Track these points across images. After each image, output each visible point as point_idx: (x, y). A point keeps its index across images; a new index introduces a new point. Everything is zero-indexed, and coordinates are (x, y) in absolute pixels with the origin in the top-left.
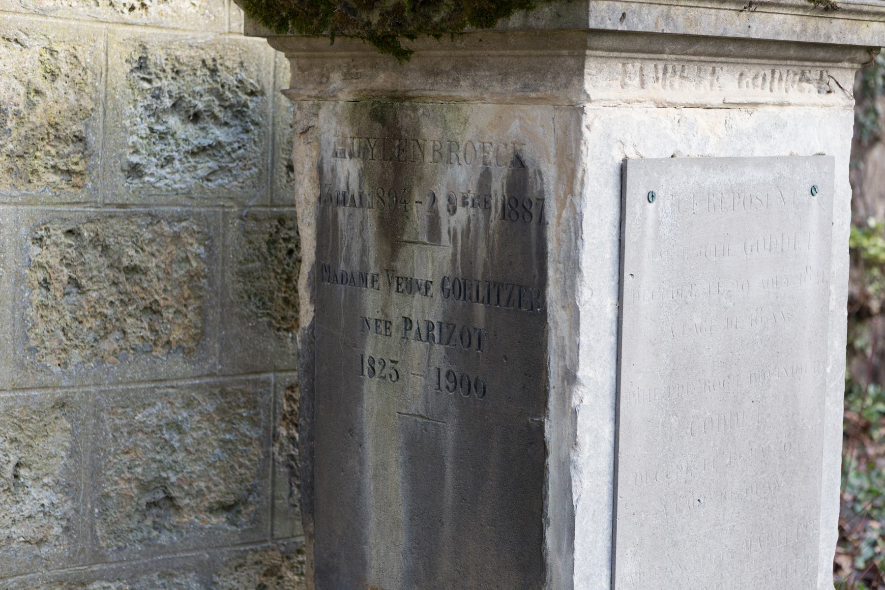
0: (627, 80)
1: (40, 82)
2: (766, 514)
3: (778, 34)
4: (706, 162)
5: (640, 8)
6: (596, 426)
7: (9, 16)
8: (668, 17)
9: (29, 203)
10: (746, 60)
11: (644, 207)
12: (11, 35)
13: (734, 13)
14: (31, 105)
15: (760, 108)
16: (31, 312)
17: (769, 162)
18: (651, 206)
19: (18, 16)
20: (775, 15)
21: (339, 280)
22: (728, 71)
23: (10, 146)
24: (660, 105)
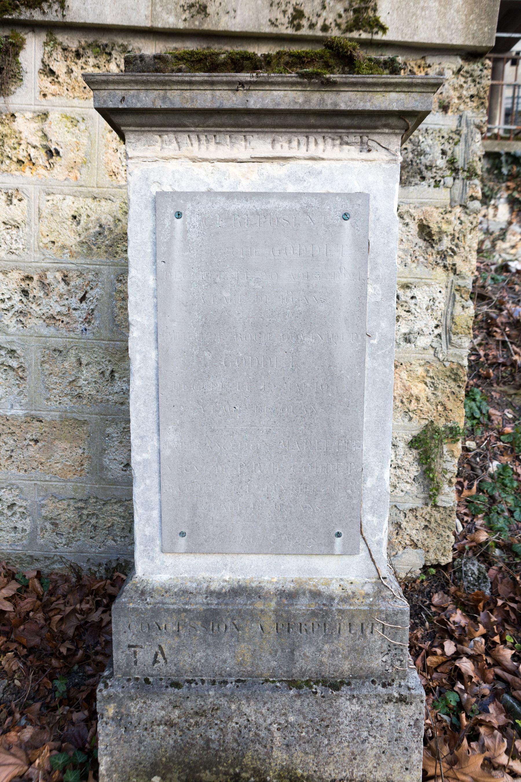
0: (164, 146)
2: (303, 427)
3: (278, 104)
4: (230, 196)
5: (138, 93)
6: (144, 350)
7: (105, 190)
8: (164, 98)
9: (114, 265)
10: (273, 130)
11: (172, 221)
12: (106, 197)
13: (229, 92)
14: (116, 226)
15: (292, 164)
16: (116, 310)
17: (296, 196)
18: (179, 221)
19: (109, 189)
20: (274, 92)
21: (500, 343)
22: (259, 138)
23: (107, 242)
24: (194, 160)
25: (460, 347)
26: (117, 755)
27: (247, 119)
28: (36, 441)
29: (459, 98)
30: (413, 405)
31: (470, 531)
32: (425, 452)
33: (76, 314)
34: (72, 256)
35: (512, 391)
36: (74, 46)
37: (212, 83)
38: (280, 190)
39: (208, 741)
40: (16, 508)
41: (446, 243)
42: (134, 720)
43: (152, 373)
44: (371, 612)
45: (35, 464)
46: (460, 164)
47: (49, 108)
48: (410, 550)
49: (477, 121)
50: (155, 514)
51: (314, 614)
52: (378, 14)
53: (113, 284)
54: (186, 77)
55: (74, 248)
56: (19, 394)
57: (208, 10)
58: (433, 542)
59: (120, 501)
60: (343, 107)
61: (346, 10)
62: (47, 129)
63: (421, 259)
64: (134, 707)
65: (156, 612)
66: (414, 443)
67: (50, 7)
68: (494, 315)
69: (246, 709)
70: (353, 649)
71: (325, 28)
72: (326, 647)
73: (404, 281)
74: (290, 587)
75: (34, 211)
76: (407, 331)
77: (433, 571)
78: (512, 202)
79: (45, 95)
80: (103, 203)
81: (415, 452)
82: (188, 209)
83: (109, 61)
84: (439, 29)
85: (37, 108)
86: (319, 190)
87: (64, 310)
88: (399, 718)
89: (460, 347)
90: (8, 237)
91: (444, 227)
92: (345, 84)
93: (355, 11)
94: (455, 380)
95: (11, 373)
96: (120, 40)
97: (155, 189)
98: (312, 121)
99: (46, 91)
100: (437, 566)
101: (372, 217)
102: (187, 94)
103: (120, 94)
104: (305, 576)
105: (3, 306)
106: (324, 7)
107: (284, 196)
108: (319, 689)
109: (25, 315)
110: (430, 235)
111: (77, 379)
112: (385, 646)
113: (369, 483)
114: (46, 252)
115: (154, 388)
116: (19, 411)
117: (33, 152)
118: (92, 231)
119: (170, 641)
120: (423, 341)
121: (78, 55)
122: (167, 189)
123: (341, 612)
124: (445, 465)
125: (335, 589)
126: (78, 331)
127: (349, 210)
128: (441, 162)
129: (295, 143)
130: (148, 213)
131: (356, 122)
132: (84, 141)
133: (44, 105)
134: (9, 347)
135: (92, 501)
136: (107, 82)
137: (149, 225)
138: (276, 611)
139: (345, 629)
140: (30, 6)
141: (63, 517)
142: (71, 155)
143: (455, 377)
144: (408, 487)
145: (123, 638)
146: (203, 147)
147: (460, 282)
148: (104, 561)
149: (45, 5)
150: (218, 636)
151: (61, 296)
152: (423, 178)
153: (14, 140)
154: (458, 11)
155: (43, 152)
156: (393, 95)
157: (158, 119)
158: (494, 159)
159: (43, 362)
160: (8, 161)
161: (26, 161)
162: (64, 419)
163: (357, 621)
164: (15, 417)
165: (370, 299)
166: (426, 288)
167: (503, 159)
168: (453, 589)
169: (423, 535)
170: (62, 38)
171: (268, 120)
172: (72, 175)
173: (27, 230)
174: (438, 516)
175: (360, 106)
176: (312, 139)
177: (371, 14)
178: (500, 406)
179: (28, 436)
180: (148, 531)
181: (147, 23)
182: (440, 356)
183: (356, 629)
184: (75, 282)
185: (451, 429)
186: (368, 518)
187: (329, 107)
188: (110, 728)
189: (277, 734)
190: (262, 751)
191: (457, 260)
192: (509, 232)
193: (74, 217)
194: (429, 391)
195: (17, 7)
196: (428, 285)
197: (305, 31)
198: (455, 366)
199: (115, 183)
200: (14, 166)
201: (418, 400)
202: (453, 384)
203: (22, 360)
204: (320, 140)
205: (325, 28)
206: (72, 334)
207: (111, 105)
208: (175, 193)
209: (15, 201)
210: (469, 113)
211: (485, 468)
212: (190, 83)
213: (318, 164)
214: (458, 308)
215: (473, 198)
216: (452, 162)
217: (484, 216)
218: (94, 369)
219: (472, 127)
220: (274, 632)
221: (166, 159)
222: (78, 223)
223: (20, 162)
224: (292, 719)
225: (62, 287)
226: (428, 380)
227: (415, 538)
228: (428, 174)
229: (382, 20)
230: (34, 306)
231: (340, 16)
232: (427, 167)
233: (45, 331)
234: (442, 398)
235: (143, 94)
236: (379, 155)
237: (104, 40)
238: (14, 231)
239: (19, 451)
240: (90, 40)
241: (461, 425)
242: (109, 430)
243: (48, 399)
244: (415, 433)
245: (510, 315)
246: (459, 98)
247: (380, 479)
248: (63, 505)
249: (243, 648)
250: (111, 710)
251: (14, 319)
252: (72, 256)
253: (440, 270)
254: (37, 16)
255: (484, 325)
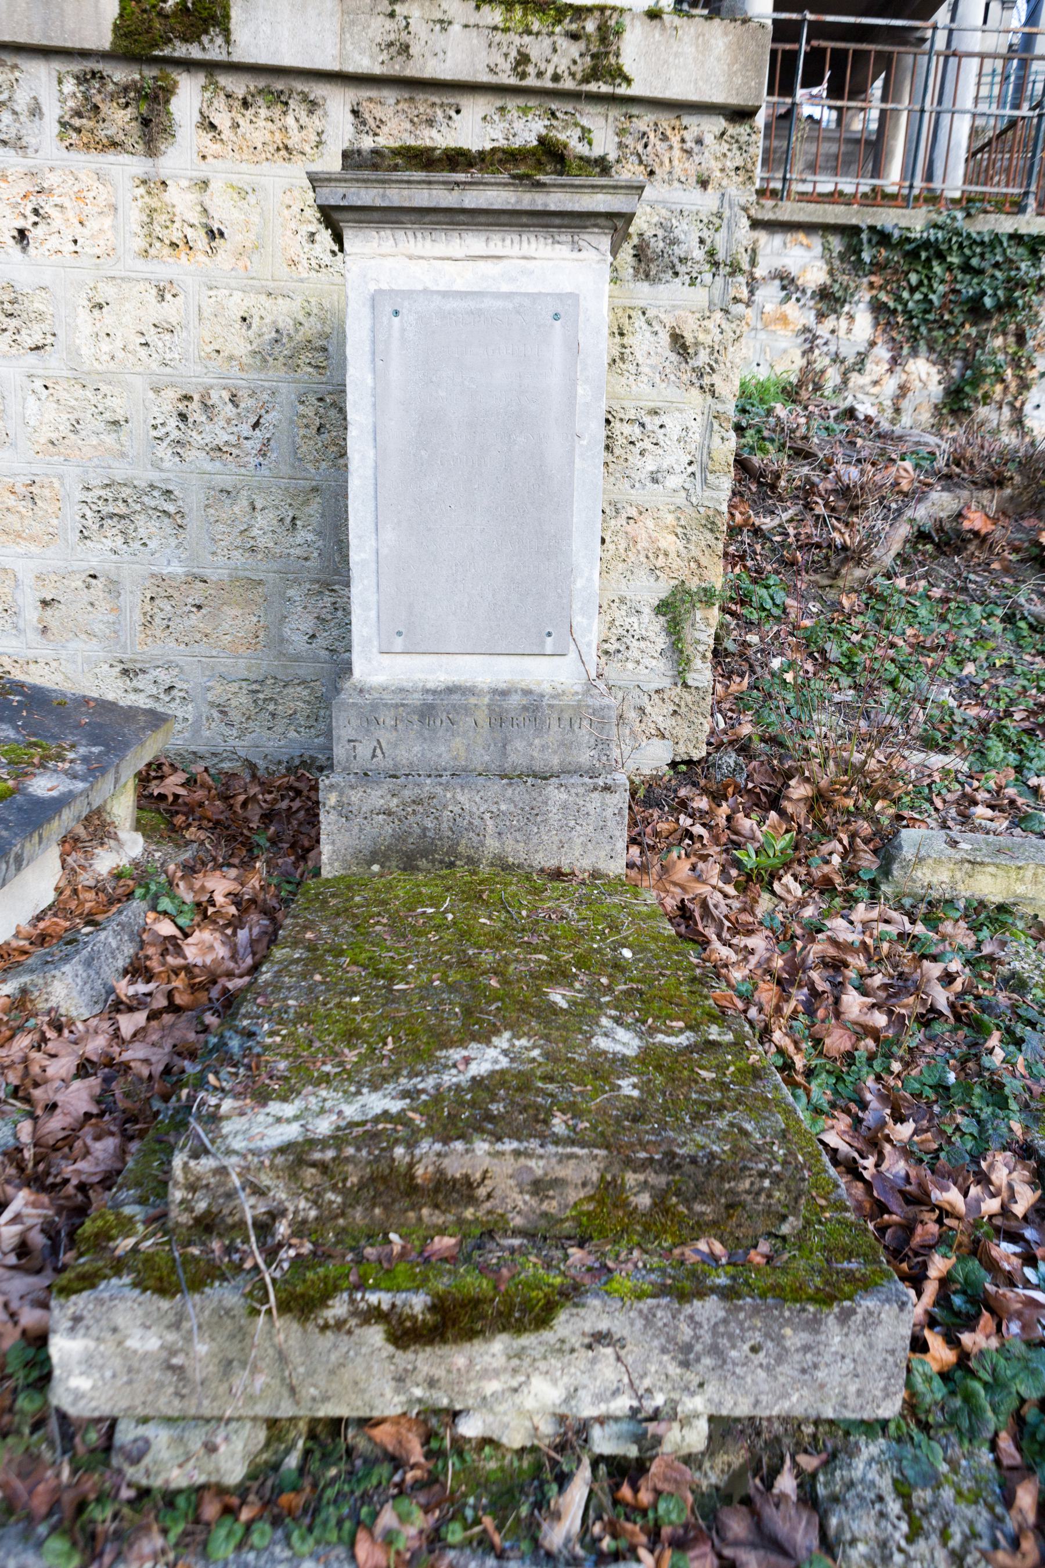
1: (301, 319)
4: (445, 294)
8: (384, 196)
14: (297, 331)
15: (505, 262)
16: (298, 440)
17: (509, 295)
24: (410, 258)
25: (717, 488)
26: (338, 844)
27: (462, 218)
28: (199, 607)
29: (722, 170)
30: (661, 562)
31: (733, 726)
32: (674, 619)
33: (248, 444)
34: (242, 369)
35: (826, 582)
36: (240, 92)
37: (430, 183)
38: (494, 289)
39: (425, 829)
40: (175, 692)
41: (703, 358)
42: (354, 809)
43: (370, 472)
44: (579, 706)
45: (198, 637)
46: (720, 257)
47: (210, 175)
48: (655, 740)
49: (743, 201)
50: (373, 614)
51: (525, 708)
52: (621, 61)
53: (294, 407)
54: (406, 175)
55: (244, 360)
56: (177, 547)
57: (411, 51)
58: (683, 731)
59: (304, 682)
60: (552, 207)
61: (582, 55)
62: (207, 204)
63: (673, 378)
64: (355, 796)
65: (374, 707)
66: (663, 608)
67: (211, 41)
68: (816, 480)
69: (460, 797)
70: (562, 744)
71: (556, 78)
72: (537, 741)
73: (652, 405)
74: (503, 686)
75: (193, 311)
76: (654, 468)
77: (683, 768)
78: (877, 308)
79: (204, 157)
80: (280, 300)
81: (662, 619)
82: (405, 307)
83: (285, 113)
84: (696, 82)
85: (195, 174)
86: (531, 289)
87: (233, 439)
88: (604, 806)
89: (717, 488)
90: (160, 344)
91: (702, 337)
92: (554, 185)
93: (594, 56)
94: (712, 531)
95: (166, 520)
96: (299, 86)
97: (372, 287)
98: (525, 220)
99: (205, 152)
100: (689, 762)
101: (582, 318)
102: (406, 192)
103: (341, 191)
104: (517, 678)
105: (155, 433)
106: (555, 50)
107: (498, 295)
108: (530, 780)
109: (183, 445)
110: (684, 347)
111: (250, 526)
112: (592, 742)
113: (580, 583)
114: (209, 364)
115: (371, 488)
116: (177, 569)
117: (190, 232)
118: (267, 337)
119: (388, 735)
120: (673, 482)
121: (245, 104)
122: (384, 286)
123: (551, 706)
124: (698, 635)
125: (546, 688)
126: (251, 467)
127: (559, 310)
128: (699, 254)
129: (508, 242)
130: (366, 311)
131: (566, 221)
132: (255, 219)
133: (204, 170)
134: (164, 486)
135: (270, 681)
136: (329, 180)
137: (367, 323)
138: (489, 706)
139: (554, 723)
140: (185, 40)
141: (234, 703)
142: (239, 237)
143: (711, 526)
144: (654, 662)
145: (343, 732)
146: (420, 244)
147: (720, 407)
148: (285, 758)
149: (205, 39)
150: (434, 731)
151: (229, 421)
152: (676, 274)
153: (165, 217)
154: (719, 60)
155: (202, 233)
156: (600, 196)
157: (376, 216)
158: (851, 236)
159: (207, 506)
160: (158, 244)
161: (181, 244)
162: (234, 579)
163: (566, 716)
164: (172, 577)
165: (580, 400)
166: (677, 414)
167: (864, 236)
168: (703, 782)
169: (671, 722)
170: (225, 80)
171: (482, 219)
172: (240, 264)
173: (185, 334)
174: (689, 698)
175: (569, 207)
176: (524, 237)
177: (612, 60)
178: (802, 597)
179: (190, 600)
180: (365, 631)
181: (332, 65)
182: (694, 500)
183: (565, 723)
184: (246, 403)
185: (705, 590)
186: (578, 620)
187: (540, 208)
188: (333, 816)
189: (489, 822)
190: (475, 839)
191: (716, 379)
192: (871, 358)
193: (244, 319)
194: (680, 544)
195: (170, 40)
196: (680, 411)
197: (531, 81)
198: (711, 513)
199: (295, 275)
200: (167, 251)
201: (666, 555)
202: (709, 536)
203: (180, 503)
204: (533, 239)
205: (556, 78)
206: (243, 471)
207: (332, 202)
208: (392, 291)
209: (168, 296)
210: (733, 191)
211: (765, 665)
212: (409, 182)
213: (530, 265)
214: (716, 439)
215: (736, 300)
216: (711, 253)
217: (833, 332)
218: (271, 515)
219: (737, 209)
220: (487, 726)
221: (383, 256)
222: (249, 327)
223: (174, 245)
224: (503, 807)
225: (229, 410)
226: (679, 530)
227: (662, 727)
228: (681, 269)
229: (625, 69)
230: (194, 434)
231: (575, 62)
232: (681, 260)
233: (209, 466)
234: (695, 552)
235: (363, 192)
236: (589, 254)
237: (279, 85)
238: (167, 336)
239: (178, 620)
240: (261, 83)
241: (718, 586)
242: (291, 593)
243: (214, 553)
244: (663, 595)
245: (838, 478)
246: (722, 170)
247: (589, 580)
248: (234, 687)
249: (458, 743)
250: (332, 799)
251: (170, 451)
252: (242, 369)
253: (695, 392)
254: (195, 52)
255: (801, 494)
